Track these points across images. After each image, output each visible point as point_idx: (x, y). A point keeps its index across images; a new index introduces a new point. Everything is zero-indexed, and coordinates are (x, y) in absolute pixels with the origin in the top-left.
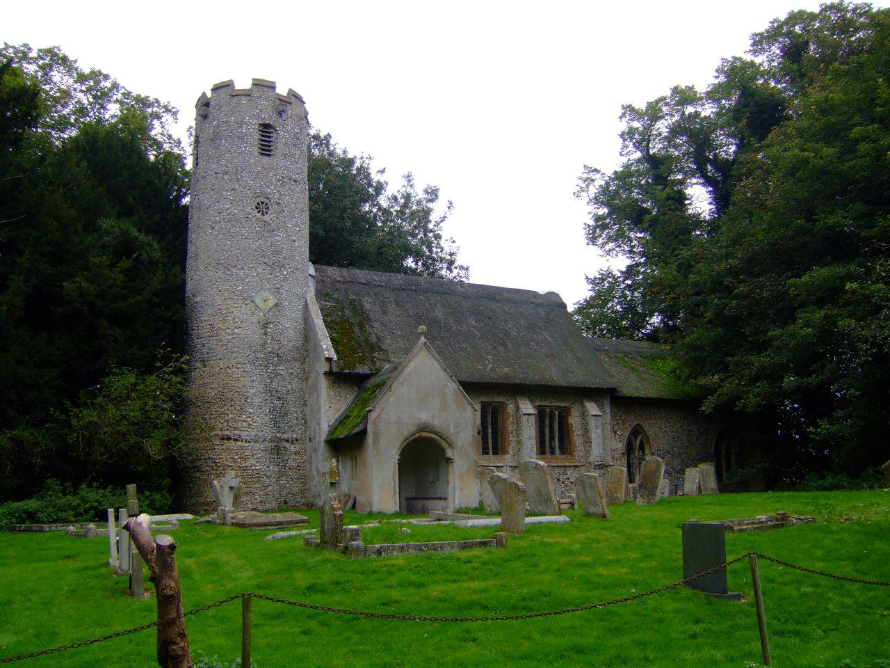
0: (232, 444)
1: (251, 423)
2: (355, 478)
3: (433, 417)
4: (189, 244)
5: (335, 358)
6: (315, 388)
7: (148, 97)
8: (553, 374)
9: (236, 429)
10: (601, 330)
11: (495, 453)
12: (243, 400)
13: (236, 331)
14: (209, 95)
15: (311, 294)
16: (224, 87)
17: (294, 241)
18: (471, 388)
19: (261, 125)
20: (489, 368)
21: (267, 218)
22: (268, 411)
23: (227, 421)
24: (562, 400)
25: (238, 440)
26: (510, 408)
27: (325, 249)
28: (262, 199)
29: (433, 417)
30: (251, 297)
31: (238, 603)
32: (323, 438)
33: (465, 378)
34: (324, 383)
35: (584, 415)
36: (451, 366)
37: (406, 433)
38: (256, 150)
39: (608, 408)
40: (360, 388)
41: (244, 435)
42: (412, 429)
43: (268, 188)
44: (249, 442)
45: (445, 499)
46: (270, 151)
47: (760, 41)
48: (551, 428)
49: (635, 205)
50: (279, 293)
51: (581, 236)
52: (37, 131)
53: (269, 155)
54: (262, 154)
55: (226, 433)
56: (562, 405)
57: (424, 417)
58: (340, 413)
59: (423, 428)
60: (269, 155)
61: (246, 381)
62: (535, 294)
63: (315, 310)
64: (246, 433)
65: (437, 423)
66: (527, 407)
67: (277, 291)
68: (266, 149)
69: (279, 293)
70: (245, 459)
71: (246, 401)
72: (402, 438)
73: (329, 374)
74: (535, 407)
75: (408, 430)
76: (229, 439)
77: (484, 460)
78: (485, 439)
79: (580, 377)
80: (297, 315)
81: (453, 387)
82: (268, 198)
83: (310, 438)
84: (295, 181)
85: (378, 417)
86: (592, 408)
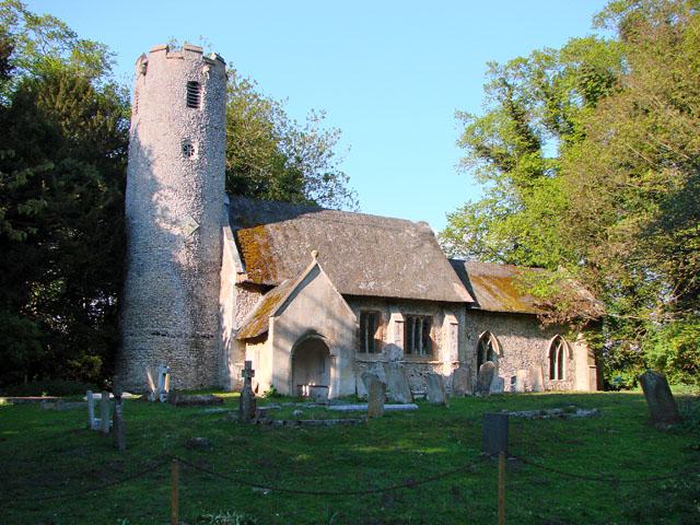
0: (160, 338)
4: (128, 178)
8: (419, 290)
10: (68, 306)
11: (371, 351)
18: (352, 300)
19: (189, 82)
20: (367, 287)
33: (352, 291)
36: (340, 284)
39: (463, 318)
41: (170, 331)
45: (327, 387)
47: (600, 20)
48: (417, 333)
49: (510, 147)
52: (118, 398)
56: (427, 314)
59: (312, 332)
74: (404, 316)
76: (158, 334)
77: (358, 357)
78: (363, 339)
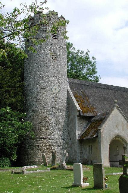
0: (44, 140)
1: (51, 133)
2: (91, 153)
3: (120, 132)
6: (73, 121)
9: (46, 135)
12: (49, 125)
13: (46, 100)
14: (67, 41)
15: (69, 88)
17: (64, 69)
21: (55, 61)
22: (57, 128)
23: (43, 132)
25: (47, 139)
28: (54, 54)
29: (120, 132)
30: (51, 88)
34: (77, 118)
37: (112, 138)
40: (88, 121)
43: (56, 50)
44: (51, 140)
46: (56, 37)
50: (60, 87)
53: (56, 39)
54: (53, 38)
55: (42, 136)
57: (117, 132)
59: (118, 136)
60: (56, 39)
61: (49, 118)
63: (70, 91)
64: (50, 136)
67: (59, 87)
69: (60, 87)
70: (49, 146)
71: (50, 125)
72: (110, 140)
75: (112, 137)
80: (66, 95)
82: (56, 54)
83: (71, 139)
84: (64, 48)
85: (103, 131)
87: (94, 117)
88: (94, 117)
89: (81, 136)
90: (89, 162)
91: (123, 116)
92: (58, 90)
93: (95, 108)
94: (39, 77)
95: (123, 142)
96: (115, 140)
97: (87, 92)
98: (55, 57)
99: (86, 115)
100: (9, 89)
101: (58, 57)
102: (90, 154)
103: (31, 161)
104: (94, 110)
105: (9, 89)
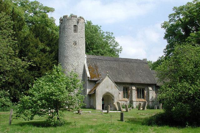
5: (90, 77)
6: (86, 83)
7: (52, 10)
15: (85, 62)
16: (65, 17)
21: (75, 46)
24: (143, 86)
26: (130, 88)
27: (89, 49)
29: (109, 91)
31: (12, 123)
32: (87, 94)
34: (87, 81)
35: (148, 90)
37: (103, 94)
38: (73, 31)
42: (105, 93)
51: (163, 38)
56: (143, 87)
57: (107, 90)
58: (39, 121)
59: (108, 93)
62: (140, 60)
65: (110, 92)
66: (134, 88)
68: (75, 31)
73: (89, 80)
79: (148, 81)
81: (114, 84)
85: (98, 90)
86: (150, 88)
87: (98, 81)
88: (98, 81)
89: (90, 92)
90: (92, 107)
91: (112, 81)
92: (77, 64)
93: (100, 75)
94: (65, 57)
95: (112, 96)
96: (106, 95)
97: (98, 64)
98: (75, 43)
99: (92, 80)
100: (45, 66)
101: (77, 44)
102: (139, 109)
103: (30, 62)
104: (100, 76)
105: (45, 66)
